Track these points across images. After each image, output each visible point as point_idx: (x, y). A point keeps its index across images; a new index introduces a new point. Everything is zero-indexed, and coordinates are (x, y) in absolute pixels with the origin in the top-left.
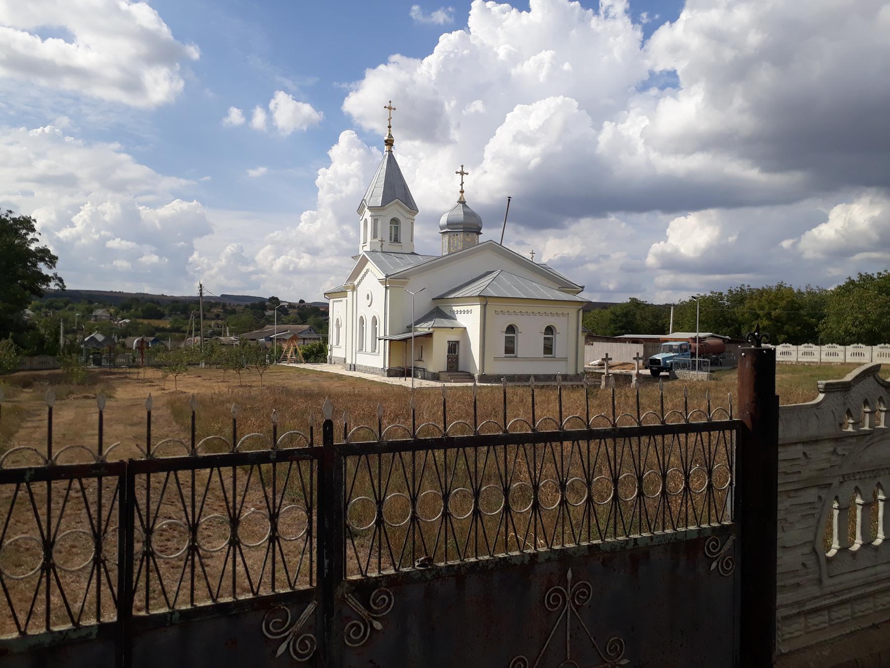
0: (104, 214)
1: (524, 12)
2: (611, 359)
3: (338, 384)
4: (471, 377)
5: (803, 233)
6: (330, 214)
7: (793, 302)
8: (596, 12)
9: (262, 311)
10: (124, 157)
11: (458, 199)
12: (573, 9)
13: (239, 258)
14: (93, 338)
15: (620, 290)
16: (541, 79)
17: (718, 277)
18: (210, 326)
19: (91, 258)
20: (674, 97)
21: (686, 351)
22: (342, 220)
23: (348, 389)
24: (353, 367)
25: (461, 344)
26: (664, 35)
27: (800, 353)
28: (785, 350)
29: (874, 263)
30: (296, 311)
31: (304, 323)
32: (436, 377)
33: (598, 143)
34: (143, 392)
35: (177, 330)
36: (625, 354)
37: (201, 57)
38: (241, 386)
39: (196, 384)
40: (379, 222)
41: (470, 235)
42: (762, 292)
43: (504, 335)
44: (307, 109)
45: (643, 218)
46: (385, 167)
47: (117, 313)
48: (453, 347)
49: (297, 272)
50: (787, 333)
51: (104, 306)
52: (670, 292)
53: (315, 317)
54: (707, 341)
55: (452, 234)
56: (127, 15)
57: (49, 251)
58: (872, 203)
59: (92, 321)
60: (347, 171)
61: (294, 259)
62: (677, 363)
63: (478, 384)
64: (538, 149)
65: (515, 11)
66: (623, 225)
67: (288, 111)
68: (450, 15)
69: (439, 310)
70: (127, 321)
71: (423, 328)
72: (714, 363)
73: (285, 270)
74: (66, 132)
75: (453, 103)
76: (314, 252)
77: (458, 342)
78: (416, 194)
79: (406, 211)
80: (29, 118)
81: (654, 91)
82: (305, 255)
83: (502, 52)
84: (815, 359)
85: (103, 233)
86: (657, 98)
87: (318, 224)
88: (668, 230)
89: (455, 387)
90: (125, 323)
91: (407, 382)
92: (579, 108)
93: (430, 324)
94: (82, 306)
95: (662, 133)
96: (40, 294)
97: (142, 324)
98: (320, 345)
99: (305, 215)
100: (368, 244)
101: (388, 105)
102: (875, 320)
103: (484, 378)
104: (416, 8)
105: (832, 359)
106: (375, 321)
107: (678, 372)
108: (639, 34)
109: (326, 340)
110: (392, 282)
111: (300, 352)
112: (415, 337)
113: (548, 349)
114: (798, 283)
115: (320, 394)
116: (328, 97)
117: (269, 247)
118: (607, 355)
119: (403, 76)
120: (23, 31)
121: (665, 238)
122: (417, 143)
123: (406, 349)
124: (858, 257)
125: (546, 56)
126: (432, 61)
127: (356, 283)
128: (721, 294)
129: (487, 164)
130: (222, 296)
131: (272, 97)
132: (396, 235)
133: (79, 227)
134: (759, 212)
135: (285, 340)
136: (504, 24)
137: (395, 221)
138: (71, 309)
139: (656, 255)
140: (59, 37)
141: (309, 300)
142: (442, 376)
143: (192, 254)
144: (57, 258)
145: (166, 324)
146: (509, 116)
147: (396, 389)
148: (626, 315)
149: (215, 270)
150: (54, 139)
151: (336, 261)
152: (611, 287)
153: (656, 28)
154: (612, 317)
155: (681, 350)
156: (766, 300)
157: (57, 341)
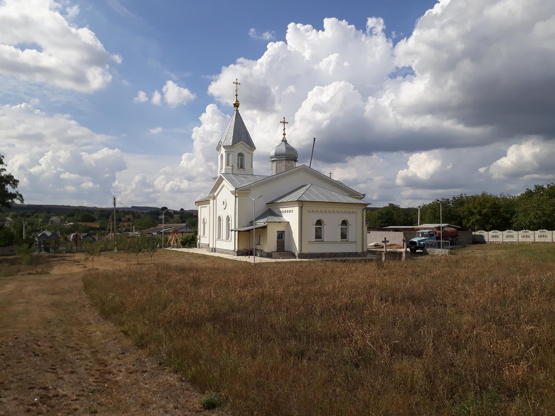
0: (60, 157)
1: (320, 31)
2: (388, 241)
3: (203, 261)
4: (293, 255)
5: (492, 163)
6: (201, 156)
7: (495, 204)
8: (364, 31)
9: (156, 216)
10: (73, 122)
11: (282, 139)
12: (351, 30)
13: (144, 183)
14: (44, 234)
15: (381, 199)
16: (330, 72)
17: (440, 191)
18: (124, 226)
19: (50, 185)
20: (411, 81)
21: (433, 235)
22: (209, 158)
23: (210, 265)
24: (214, 250)
25: (286, 233)
26: (403, 46)
27: (505, 236)
28: (495, 234)
29: (546, 180)
30: (178, 215)
31: (183, 222)
32: (269, 255)
33: (365, 111)
34: (76, 269)
35: (104, 229)
36: (395, 238)
37: (122, 61)
38: (138, 264)
39: (103, 264)
40: (231, 156)
41: (290, 162)
42: (474, 198)
43: (315, 226)
44: (186, 92)
45: (394, 155)
46: (234, 120)
47: (65, 219)
48: (281, 235)
49: (180, 191)
50: (492, 224)
51: (58, 215)
52: (411, 200)
53: (189, 219)
54: (445, 229)
55: (278, 162)
56: (76, 36)
57: (13, 177)
58: (533, 144)
59: (50, 224)
60: (212, 127)
61: (179, 184)
62: (427, 244)
63: (298, 260)
64: (328, 115)
65: (315, 31)
66: (382, 160)
67: (174, 93)
68: (273, 35)
69: (271, 210)
70: (72, 223)
71: (261, 223)
72: (452, 243)
73: (172, 190)
74: (36, 107)
75: (276, 88)
76: (190, 179)
77: (284, 232)
78: (255, 140)
79: (247, 147)
80: (12, 99)
81: (400, 78)
82: (185, 181)
83: (307, 55)
84: (515, 240)
85: (58, 169)
86: (400, 82)
87: (193, 162)
88: (408, 163)
89: (283, 262)
90: (70, 225)
91: (250, 259)
92: (354, 89)
93: (265, 220)
94: (43, 215)
95: (406, 102)
96: (9, 206)
97: (81, 225)
98: (193, 236)
99: (185, 156)
100: (224, 169)
101: (235, 81)
102: (549, 214)
103: (301, 256)
104: (252, 30)
105: (525, 240)
106: (228, 219)
107: (428, 250)
108: (391, 44)
109: (196, 233)
110: (239, 192)
111: (179, 241)
112: (256, 228)
113: (344, 236)
114: (495, 192)
115: (191, 269)
116: (199, 83)
117: (163, 176)
118: (385, 238)
119: (245, 71)
120: (10, 45)
121: (408, 167)
122: (255, 112)
123: (249, 237)
124: (527, 177)
125: (333, 57)
126: (264, 59)
127: (215, 194)
128: (448, 199)
129: (297, 124)
130: (133, 207)
131: (165, 84)
132: (241, 164)
133: (44, 166)
134: (464, 151)
135: (170, 233)
136: (308, 38)
137: (241, 155)
138: (37, 217)
139: (402, 178)
140: (32, 49)
141: (187, 209)
142: (274, 255)
143: (114, 181)
144: (18, 181)
145: (96, 225)
146: (310, 93)
147: (243, 264)
148: (388, 214)
149: (129, 191)
150: (29, 112)
151: (203, 184)
152: (375, 198)
153: (399, 41)
154: (380, 215)
155: (430, 235)
156: (478, 203)
157: (22, 236)
